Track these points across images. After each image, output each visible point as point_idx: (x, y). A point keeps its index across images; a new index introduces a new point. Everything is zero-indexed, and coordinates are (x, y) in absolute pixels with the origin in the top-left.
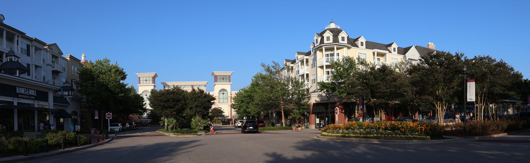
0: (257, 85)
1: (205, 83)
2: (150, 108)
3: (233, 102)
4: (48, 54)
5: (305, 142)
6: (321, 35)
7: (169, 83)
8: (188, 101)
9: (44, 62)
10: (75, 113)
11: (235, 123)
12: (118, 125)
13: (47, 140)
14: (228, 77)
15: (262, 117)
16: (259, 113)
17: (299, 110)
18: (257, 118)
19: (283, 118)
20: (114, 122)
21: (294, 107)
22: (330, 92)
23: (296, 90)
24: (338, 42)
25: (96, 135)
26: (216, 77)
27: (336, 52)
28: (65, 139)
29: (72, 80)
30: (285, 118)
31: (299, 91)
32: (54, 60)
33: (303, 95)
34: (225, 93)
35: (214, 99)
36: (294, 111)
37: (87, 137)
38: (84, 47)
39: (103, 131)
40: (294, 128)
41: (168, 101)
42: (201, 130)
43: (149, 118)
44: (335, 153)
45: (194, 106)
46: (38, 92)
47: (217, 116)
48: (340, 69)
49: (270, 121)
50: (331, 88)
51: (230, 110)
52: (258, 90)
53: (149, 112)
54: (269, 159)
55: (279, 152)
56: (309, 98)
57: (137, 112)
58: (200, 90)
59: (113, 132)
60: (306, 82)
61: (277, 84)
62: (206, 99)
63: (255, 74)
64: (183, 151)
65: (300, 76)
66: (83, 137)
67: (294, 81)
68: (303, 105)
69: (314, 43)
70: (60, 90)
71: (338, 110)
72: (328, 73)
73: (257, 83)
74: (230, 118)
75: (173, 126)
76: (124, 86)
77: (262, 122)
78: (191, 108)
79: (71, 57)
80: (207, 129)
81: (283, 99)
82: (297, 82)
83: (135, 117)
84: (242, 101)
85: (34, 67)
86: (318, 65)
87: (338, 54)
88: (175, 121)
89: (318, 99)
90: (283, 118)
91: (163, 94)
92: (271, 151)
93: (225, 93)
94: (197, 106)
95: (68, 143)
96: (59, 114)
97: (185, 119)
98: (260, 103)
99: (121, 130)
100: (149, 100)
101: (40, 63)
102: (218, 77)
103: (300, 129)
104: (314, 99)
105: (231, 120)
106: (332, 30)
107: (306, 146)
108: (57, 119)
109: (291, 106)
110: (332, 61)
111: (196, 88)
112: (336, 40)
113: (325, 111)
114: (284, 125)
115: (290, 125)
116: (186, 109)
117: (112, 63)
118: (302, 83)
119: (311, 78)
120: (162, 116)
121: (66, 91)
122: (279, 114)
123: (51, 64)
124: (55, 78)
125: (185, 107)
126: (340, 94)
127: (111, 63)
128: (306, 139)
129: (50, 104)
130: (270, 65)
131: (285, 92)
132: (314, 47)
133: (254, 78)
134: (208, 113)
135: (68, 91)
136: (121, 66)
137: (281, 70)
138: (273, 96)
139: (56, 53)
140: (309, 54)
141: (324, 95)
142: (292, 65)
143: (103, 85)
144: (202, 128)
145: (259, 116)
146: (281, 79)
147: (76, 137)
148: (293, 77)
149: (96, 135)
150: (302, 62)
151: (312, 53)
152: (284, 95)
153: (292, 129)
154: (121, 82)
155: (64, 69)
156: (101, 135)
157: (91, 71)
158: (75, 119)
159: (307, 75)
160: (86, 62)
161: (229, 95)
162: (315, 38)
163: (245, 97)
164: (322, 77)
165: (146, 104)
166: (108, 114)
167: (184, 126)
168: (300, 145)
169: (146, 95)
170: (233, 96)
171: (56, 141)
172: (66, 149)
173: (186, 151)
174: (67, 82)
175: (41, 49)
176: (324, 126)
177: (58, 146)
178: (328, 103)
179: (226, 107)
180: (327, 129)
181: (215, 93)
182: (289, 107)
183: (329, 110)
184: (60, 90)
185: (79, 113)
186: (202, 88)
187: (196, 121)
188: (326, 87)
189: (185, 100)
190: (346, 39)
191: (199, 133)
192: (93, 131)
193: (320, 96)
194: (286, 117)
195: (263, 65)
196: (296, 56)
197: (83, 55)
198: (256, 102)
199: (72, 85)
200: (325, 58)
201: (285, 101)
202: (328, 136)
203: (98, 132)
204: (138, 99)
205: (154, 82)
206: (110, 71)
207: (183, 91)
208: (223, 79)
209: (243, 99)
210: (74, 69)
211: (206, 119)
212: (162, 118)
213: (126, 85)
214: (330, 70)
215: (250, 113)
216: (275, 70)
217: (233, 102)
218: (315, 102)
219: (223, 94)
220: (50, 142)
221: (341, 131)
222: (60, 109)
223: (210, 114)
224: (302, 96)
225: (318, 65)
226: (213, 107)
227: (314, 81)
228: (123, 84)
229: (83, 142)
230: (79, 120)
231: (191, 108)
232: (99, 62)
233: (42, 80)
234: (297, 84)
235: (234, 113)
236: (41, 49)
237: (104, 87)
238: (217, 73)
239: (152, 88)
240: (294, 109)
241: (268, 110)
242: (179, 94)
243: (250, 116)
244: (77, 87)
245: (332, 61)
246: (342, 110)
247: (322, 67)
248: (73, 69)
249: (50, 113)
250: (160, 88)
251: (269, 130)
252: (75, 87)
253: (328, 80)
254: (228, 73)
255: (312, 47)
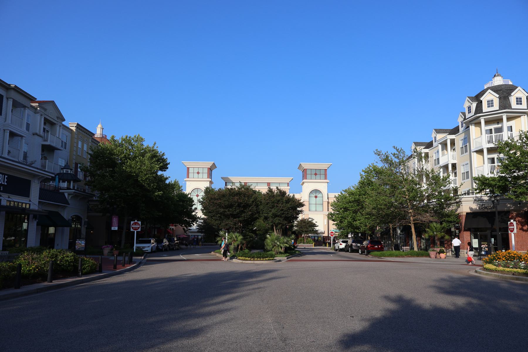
0: (369, 184)
1: (287, 180)
2: (203, 216)
3: (331, 211)
4: (38, 116)
5: (451, 280)
6: (477, 98)
7: (234, 179)
8: (261, 207)
9: (28, 128)
10: (78, 219)
11: (334, 244)
12: (149, 242)
13: (20, 265)
14: (323, 172)
15: (379, 235)
16: (372, 229)
17: (441, 224)
18: (371, 236)
19: (414, 236)
20: (143, 237)
21: (431, 219)
22: (497, 193)
23: (435, 190)
24: (510, 107)
25: (112, 258)
26: (305, 171)
27: (506, 124)
28: (54, 263)
29: (76, 164)
30: (417, 236)
31: (440, 193)
32: (47, 128)
33: (448, 199)
34: (319, 195)
35: (302, 205)
36: (431, 225)
37: (96, 260)
38: (103, 110)
39: (125, 251)
40: (432, 254)
41: (230, 206)
42: (281, 253)
43: (201, 232)
44: (512, 305)
45: (270, 214)
46: (10, 178)
47: (307, 232)
48: (515, 153)
49: (392, 242)
50: (499, 187)
51: (326, 223)
52: (369, 192)
53: (200, 222)
54: (391, 306)
55: (408, 295)
56: (459, 204)
57: (182, 222)
58: (280, 191)
59: (141, 252)
60: (452, 177)
61: (401, 182)
62: (289, 205)
63: (365, 166)
64: (251, 287)
65: (441, 167)
66: (89, 261)
67: (431, 175)
68: (448, 216)
69: (464, 114)
70: (53, 179)
71: (514, 225)
72: (492, 161)
73: (369, 180)
74: (326, 235)
75: (238, 246)
76: (162, 179)
77: (379, 243)
78: (266, 218)
79: (79, 126)
80: (290, 251)
81: (413, 206)
82: (436, 178)
83: (178, 229)
84: (347, 209)
85: (8, 134)
86: (473, 148)
87: (510, 129)
88: (241, 237)
89: (475, 206)
90: (414, 236)
91: (224, 196)
92: (394, 292)
93: (319, 195)
94: (275, 216)
95: (60, 271)
96: (45, 219)
97: (256, 235)
98: (374, 212)
99: (154, 249)
100: (202, 203)
101: (21, 130)
102: (308, 172)
103: (443, 255)
104: (467, 205)
105: (328, 238)
106: (496, 89)
107: (454, 287)
108: (43, 227)
109: (427, 217)
110: (499, 141)
111: (274, 188)
112: (505, 103)
113: (489, 226)
114: (416, 249)
115: (426, 249)
116: (257, 219)
117: (147, 143)
118: (445, 179)
119: (461, 170)
120: (221, 230)
121: (64, 182)
122: (407, 230)
123: (42, 133)
124: (46, 158)
125: (257, 215)
126: (517, 196)
127: (145, 144)
128: (455, 275)
129: (33, 201)
130: (389, 153)
131: (416, 195)
132: (465, 119)
133: (363, 174)
134: (293, 226)
135: (69, 182)
136: (160, 149)
137: (408, 159)
138: (396, 201)
139: (52, 117)
140: (455, 131)
141: (486, 198)
142: (427, 150)
143: (129, 176)
144: (282, 250)
145: (373, 233)
146: (408, 174)
147: (76, 260)
148: (429, 169)
149: (112, 258)
150: (444, 145)
151: (461, 129)
152: (414, 198)
153: (429, 256)
154: (160, 173)
155: (64, 145)
156: (120, 258)
157: (111, 153)
158: (76, 229)
159: (454, 166)
160: (104, 137)
161: (325, 199)
162: (467, 104)
163: (350, 202)
164: (481, 169)
165: (196, 209)
166: (135, 224)
167: (255, 246)
168: (443, 285)
169: (197, 196)
170: (331, 201)
171: (37, 267)
172: (55, 282)
173: (255, 286)
174: (67, 167)
175: (25, 107)
176: (487, 253)
177: (39, 276)
178: (493, 213)
179: (319, 217)
180: (494, 259)
181: (303, 196)
182: (424, 219)
183: (497, 226)
184: (53, 179)
185: (85, 219)
186: (283, 188)
187: (273, 238)
188: (489, 185)
189: (257, 206)
190: (524, 101)
191: (277, 258)
192: (106, 251)
193: (478, 200)
194: (419, 235)
195: (378, 153)
196: (433, 135)
197: (99, 126)
198: (368, 210)
199: (76, 171)
200: (485, 137)
201: (416, 208)
202: (496, 271)
203: (116, 252)
204: (183, 201)
205: (210, 175)
206: (143, 155)
207: (255, 192)
208: (316, 174)
209: (347, 205)
210: (83, 146)
211: (289, 236)
212: (221, 233)
213: (167, 178)
214: (495, 156)
215: (358, 228)
216: (397, 160)
217: (331, 211)
218: (469, 211)
219: (316, 197)
220: (25, 269)
221: (522, 264)
222: (50, 212)
223: (295, 228)
224: (446, 201)
225: (473, 148)
226: (301, 217)
227: (466, 175)
228: (162, 176)
229: (88, 269)
230: (84, 231)
231: (266, 218)
232: (127, 140)
233: (21, 159)
234: (435, 181)
235: (333, 228)
236: (25, 107)
237: (132, 179)
238: (306, 165)
239: (207, 184)
240: (432, 222)
241: (388, 223)
242: (248, 197)
243: (358, 233)
244: (85, 176)
245: (499, 141)
246: (523, 226)
247: (480, 152)
248: (80, 146)
249: (31, 216)
250: (219, 185)
251: (391, 256)
252: (80, 176)
253: (492, 173)
254: (323, 166)
255: (460, 119)
